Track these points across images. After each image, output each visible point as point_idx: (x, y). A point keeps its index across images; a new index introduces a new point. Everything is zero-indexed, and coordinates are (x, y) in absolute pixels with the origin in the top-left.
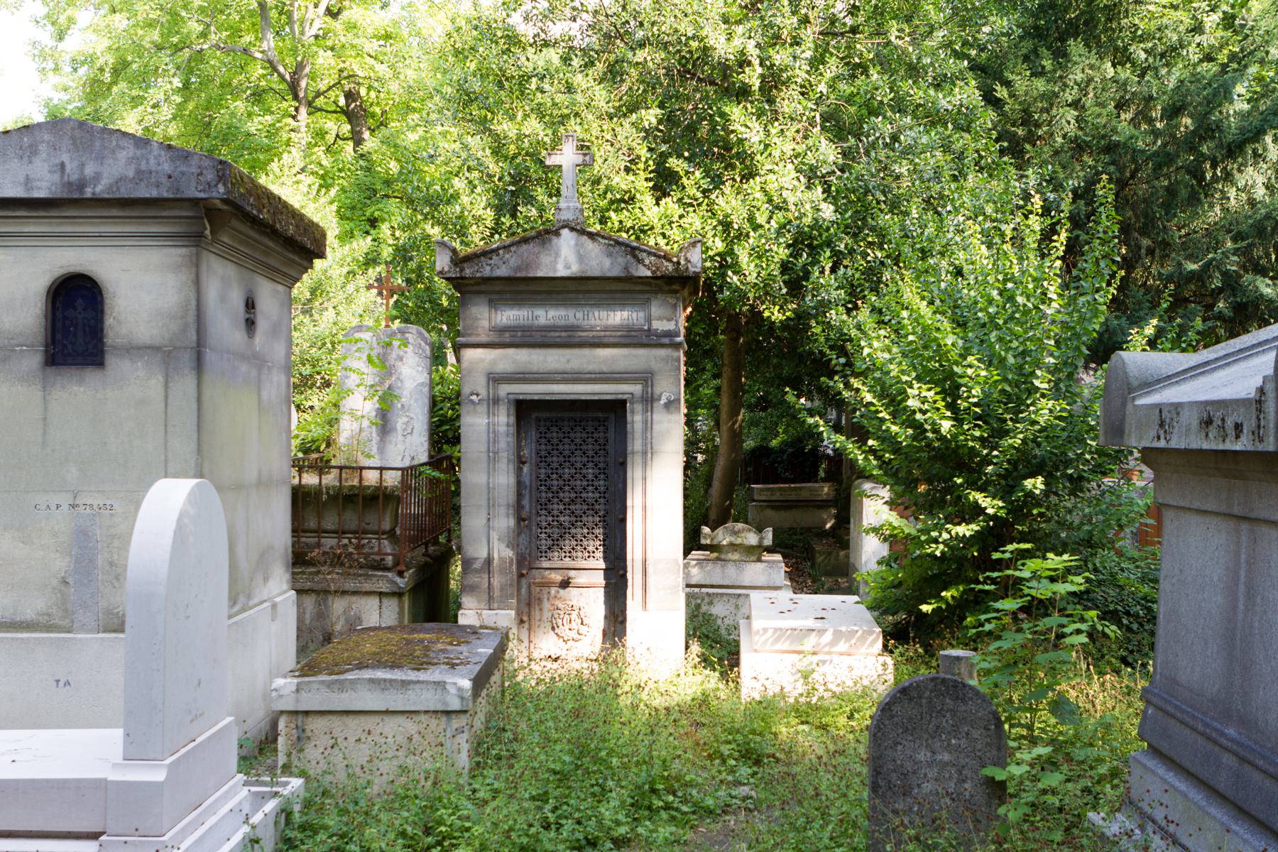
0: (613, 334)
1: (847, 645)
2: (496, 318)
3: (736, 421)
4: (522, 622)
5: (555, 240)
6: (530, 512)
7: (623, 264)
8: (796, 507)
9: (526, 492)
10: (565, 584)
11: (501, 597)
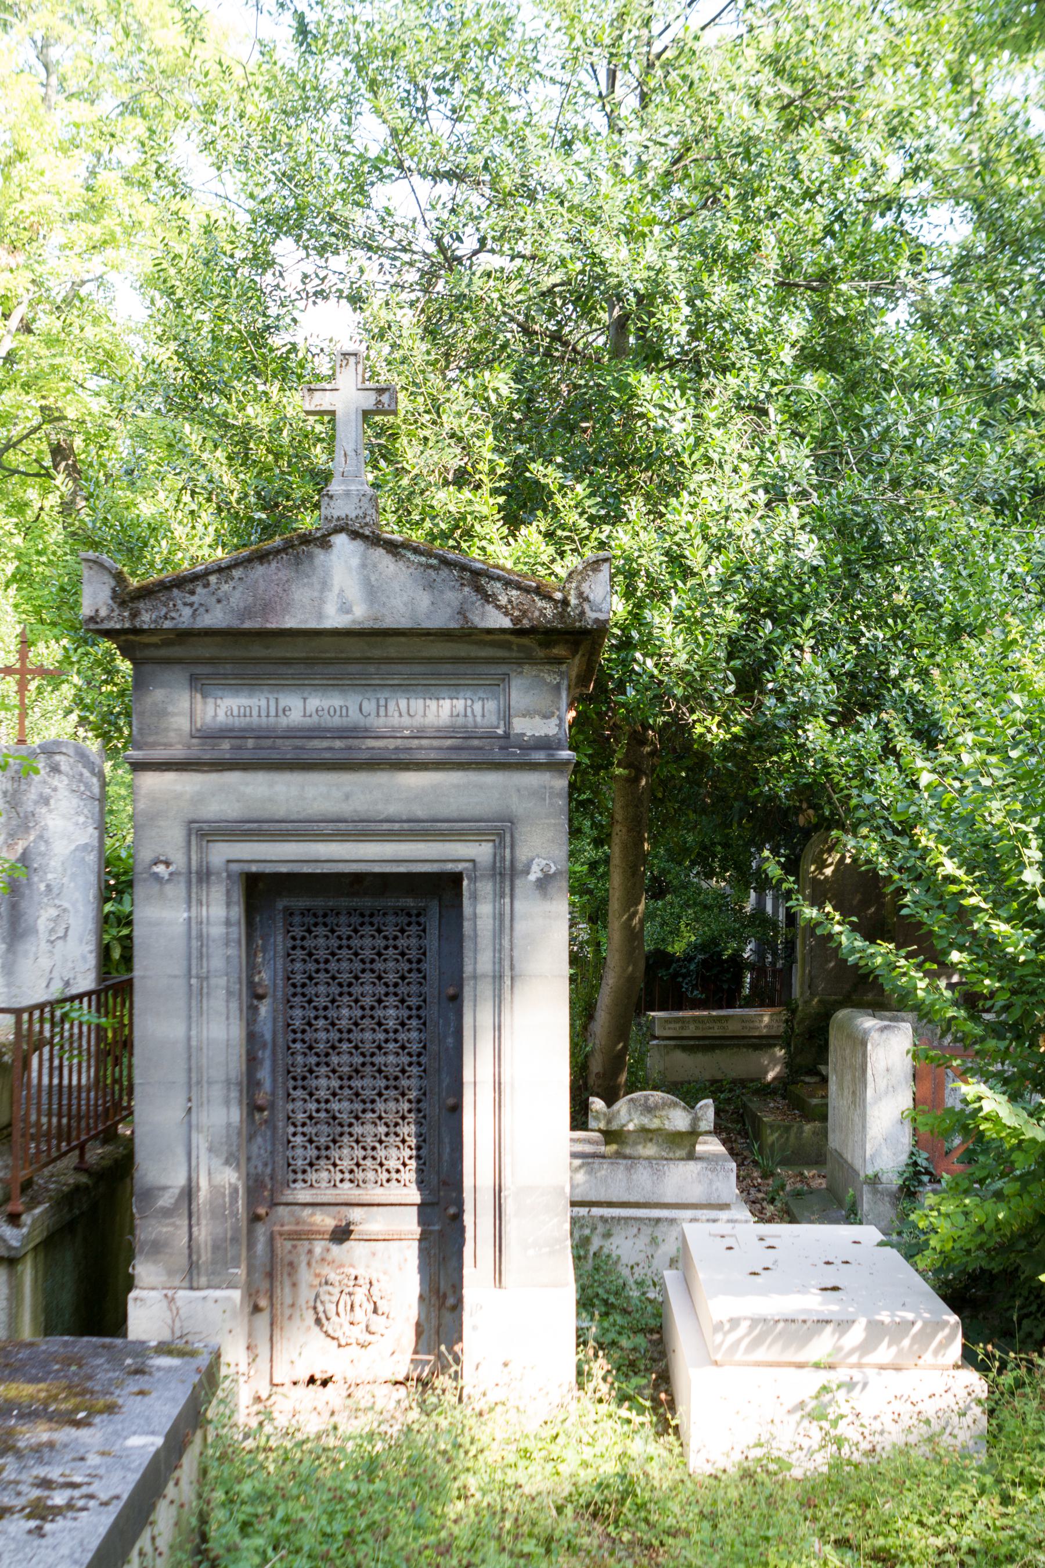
0: (436, 743)
1: (894, 1349)
2: (204, 712)
3: (635, 913)
4: (256, 1309)
5: (320, 556)
6: (273, 1094)
7: (456, 604)
8: (721, 1047)
9: (266, 1055)
10: (342, 1234)
11: (214, 1262)
